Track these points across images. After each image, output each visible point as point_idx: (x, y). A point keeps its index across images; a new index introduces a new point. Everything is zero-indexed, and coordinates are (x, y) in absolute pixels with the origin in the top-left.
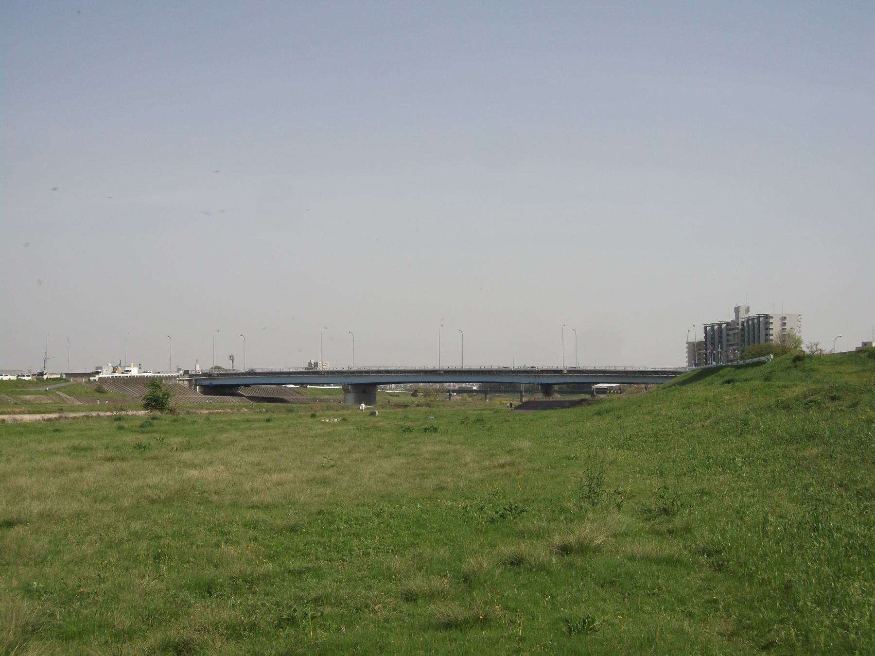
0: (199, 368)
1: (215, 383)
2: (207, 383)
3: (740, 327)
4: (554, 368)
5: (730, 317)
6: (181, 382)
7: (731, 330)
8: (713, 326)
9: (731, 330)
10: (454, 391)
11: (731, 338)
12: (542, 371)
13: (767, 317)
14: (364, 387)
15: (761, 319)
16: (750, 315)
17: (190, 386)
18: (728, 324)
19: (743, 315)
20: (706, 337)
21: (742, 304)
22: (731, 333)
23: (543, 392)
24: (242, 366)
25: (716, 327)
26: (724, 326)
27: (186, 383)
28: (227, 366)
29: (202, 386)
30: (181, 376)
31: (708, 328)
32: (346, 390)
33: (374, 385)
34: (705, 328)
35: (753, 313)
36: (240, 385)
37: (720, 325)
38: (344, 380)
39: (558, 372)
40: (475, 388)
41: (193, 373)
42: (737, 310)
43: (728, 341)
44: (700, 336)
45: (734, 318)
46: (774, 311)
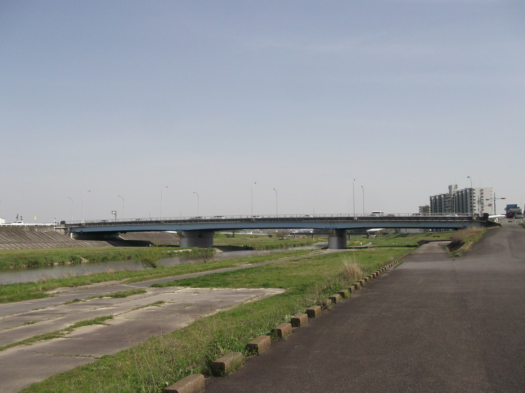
0: (71, 220)
1: (85, 230)
2: (78, 230)
3: (452, 197)
4: (347, 216)
5: (447, 191)
6: (58, 231)
7: (446, 198)
8: (435, 197)
9: (446, 198)
10: (296, 234)
11: (446, 203)
12: (336, 218)
13: (471, 190)
14: (201, 234)
15: (468, 191)
16: (458, 190)
17: (66, 233)
18: (444, 195)
19: (454, 191)
20: (431, 203)
21: (453, 185)
22: (447, 200)
23: (337, 236)
24: (122, 218)
25: (437, 197)
26: (442, 196)
27: (63, 230)
28: (110, 219)
29: (75, 233)
30: (58, 226)
31: (432, 198)
32: (180, 235)
33: (212, 231)
34: (431, 198)
35: (459, 189)
36: (118, 231)
37: (440, 196)
38: (178, 228)
39: (350, 219)
40: (311, 232)
41: (68, 223)
42: (450, 187)
43: (445, 204)
44: (427, 203)
45: (448, 193)
46: (476, 186)
